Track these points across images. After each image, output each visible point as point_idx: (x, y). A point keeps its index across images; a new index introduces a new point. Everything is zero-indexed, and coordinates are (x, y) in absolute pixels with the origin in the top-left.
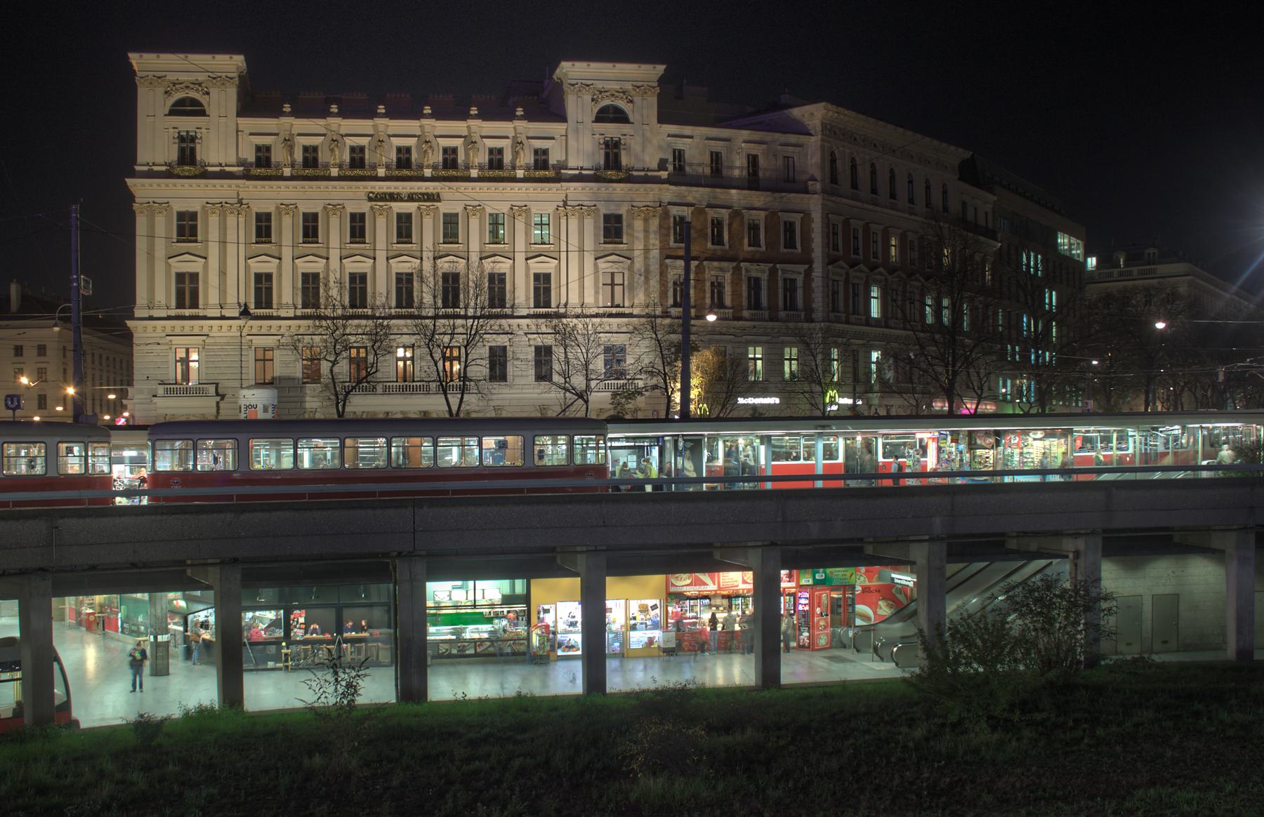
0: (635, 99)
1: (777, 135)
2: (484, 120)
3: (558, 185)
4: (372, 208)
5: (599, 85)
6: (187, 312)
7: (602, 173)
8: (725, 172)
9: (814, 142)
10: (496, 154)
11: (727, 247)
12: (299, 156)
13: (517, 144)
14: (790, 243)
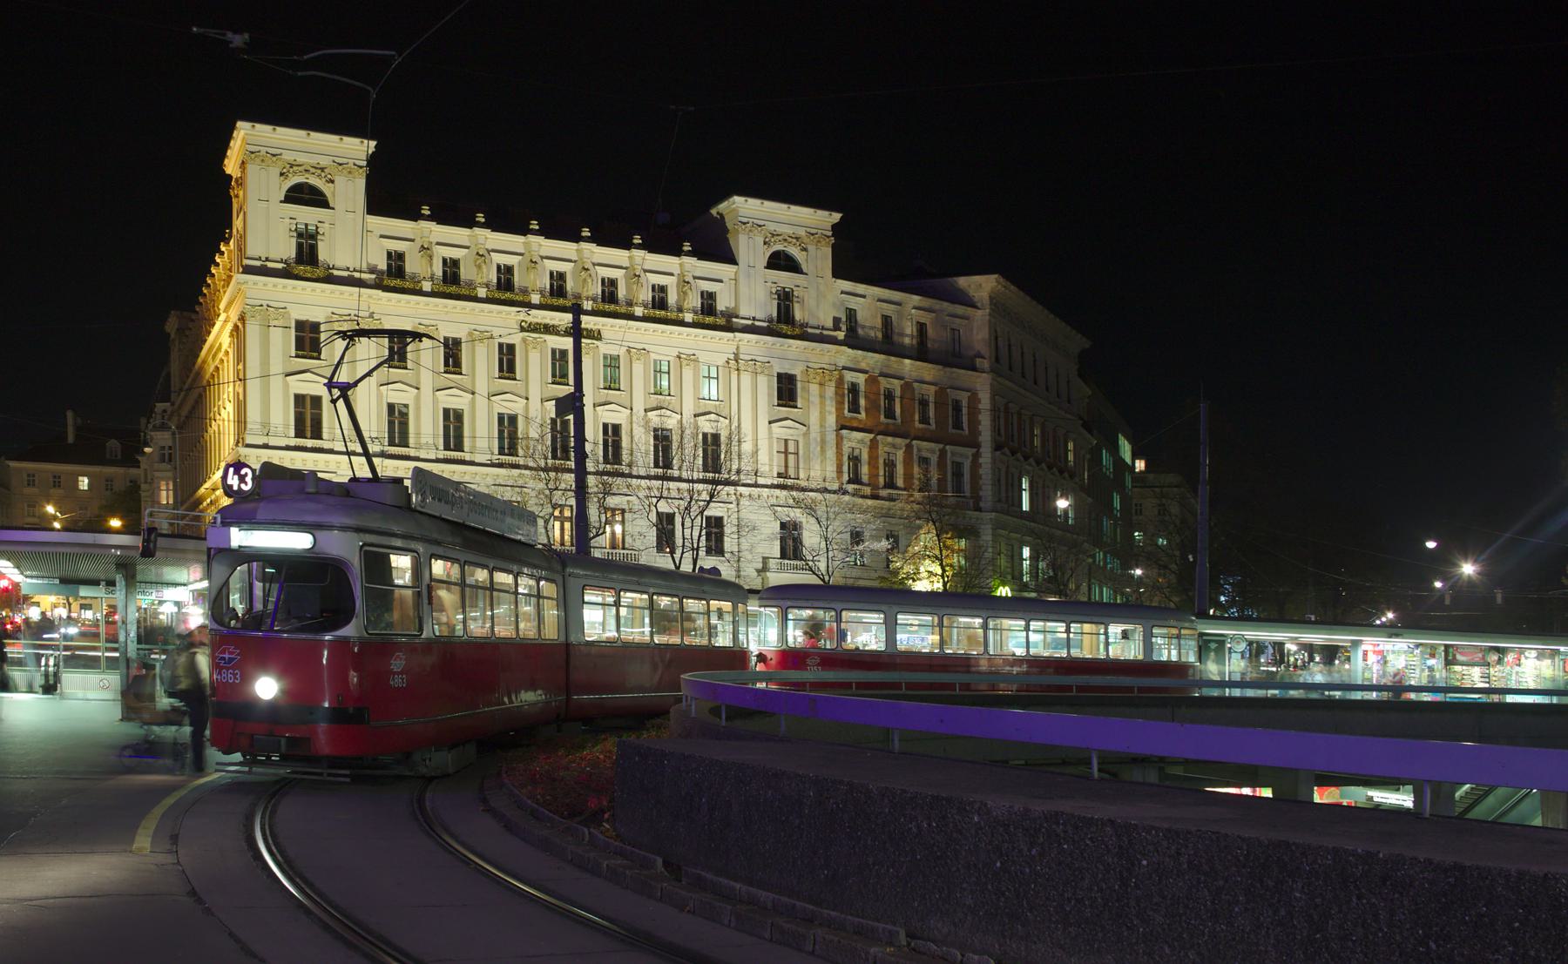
0: (810, 248)
1: (945, 304)
2: (599, 244)
3: (730, 335)
4: (524, 340)
5: (772, 227)
6: (310, 443)
7: (775, 326)
8: (895, 338)
9: (981, 316)
10: (451, 266)
11: (933, 426)
12: (438, 270)
13: (684, 283)
14: (958, 425)
